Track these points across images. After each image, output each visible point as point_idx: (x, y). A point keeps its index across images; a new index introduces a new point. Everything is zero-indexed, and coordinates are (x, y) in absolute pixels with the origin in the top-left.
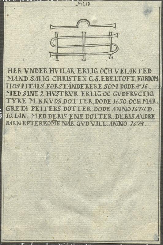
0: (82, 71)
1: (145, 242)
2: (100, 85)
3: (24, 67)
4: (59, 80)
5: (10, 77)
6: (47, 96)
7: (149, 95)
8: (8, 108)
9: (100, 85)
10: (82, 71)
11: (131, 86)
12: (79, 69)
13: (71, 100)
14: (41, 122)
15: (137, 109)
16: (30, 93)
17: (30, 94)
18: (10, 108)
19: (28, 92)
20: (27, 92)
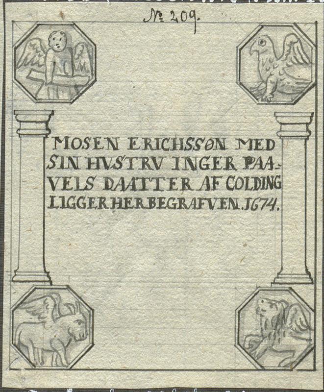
0: (139, 143)
1: (318, 248)
2: (259, 142)
3: (106, 136)
4: (178, 147)
5: (61, 138)
6: (89, 168)
7: (245, 180)
8: (81, 200)
9: (259, 142)
10: (139, 143)
11: (260, 183)
12: (131, 139)
13: (182, 20)
14: (147, 158)
15: (257, 206)
16: (66, 160)
17: (66, 165)
18: (87, 202)
19: (63, 158)
20: (59, 159)
